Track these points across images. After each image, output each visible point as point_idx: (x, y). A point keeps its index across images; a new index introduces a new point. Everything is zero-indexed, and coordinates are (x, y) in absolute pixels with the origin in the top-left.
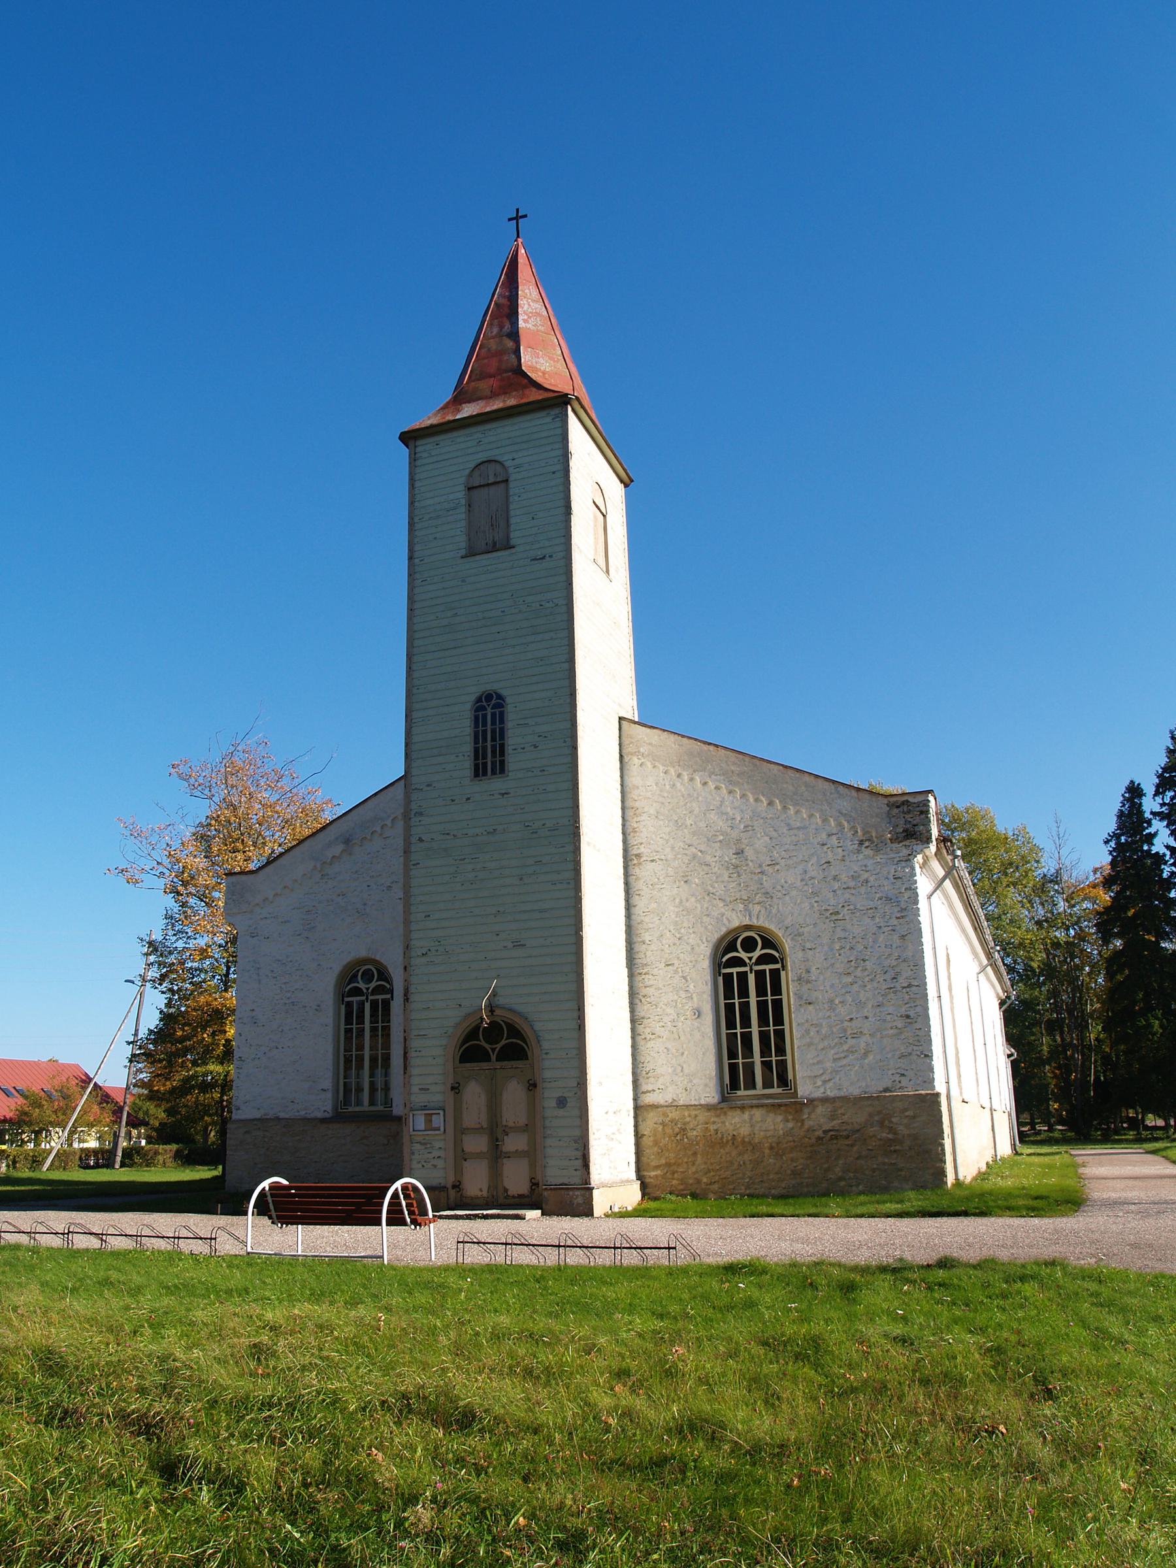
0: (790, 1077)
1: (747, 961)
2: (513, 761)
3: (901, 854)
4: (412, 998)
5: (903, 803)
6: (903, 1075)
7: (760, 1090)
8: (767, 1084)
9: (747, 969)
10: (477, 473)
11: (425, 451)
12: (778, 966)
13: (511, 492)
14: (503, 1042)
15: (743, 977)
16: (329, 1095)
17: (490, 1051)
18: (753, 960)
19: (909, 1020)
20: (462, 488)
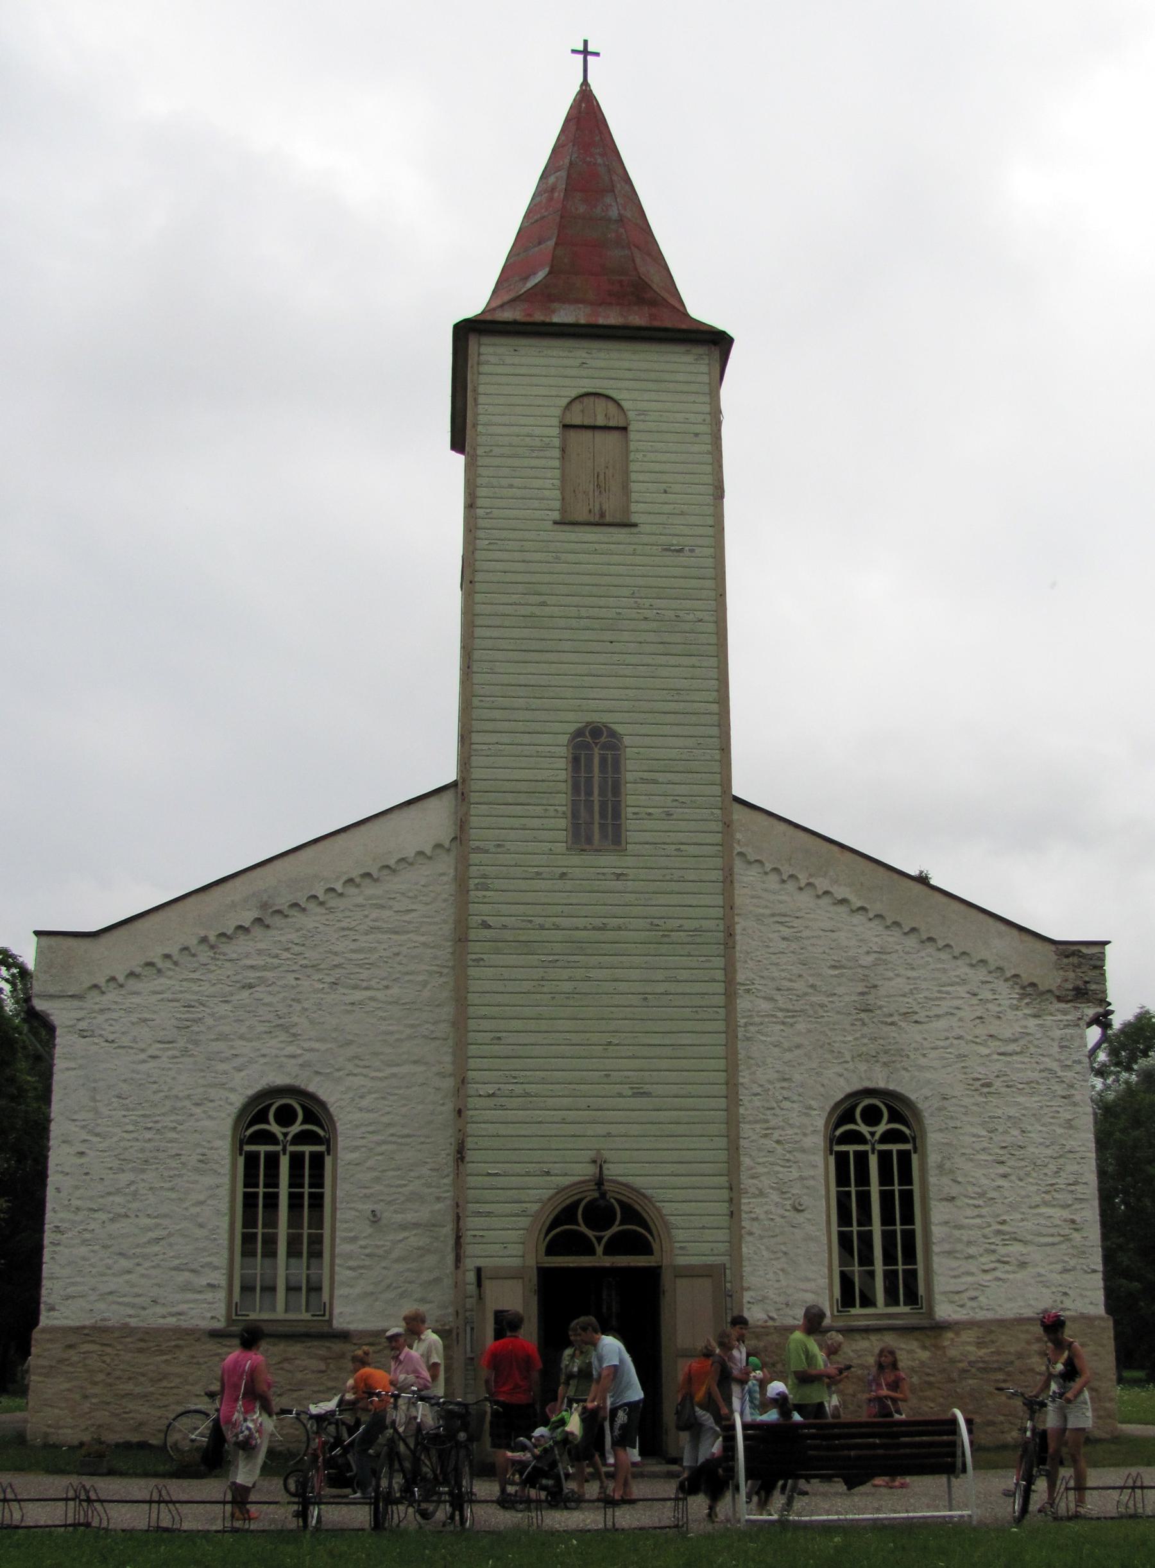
0: (921, 1291)
1: (868, 1137)
2: (635, 830)
3: (1068, 1017)
4: (470, 1155)
5: (1073, 954)
6: (1065, 1294)
7: (881, 1307)
8: (892, 1297)
9: (867, 1148)
10: (577, 407)
11: (495, 354)
12: (907, 1147)
13: (633, 446)
14: (615, 1229)
15: (862, 1158)
16: (222, 1295)
17: (594, 1240)
18: (877, 1137)
19: (1074, 1226)
20: (555, 422)
